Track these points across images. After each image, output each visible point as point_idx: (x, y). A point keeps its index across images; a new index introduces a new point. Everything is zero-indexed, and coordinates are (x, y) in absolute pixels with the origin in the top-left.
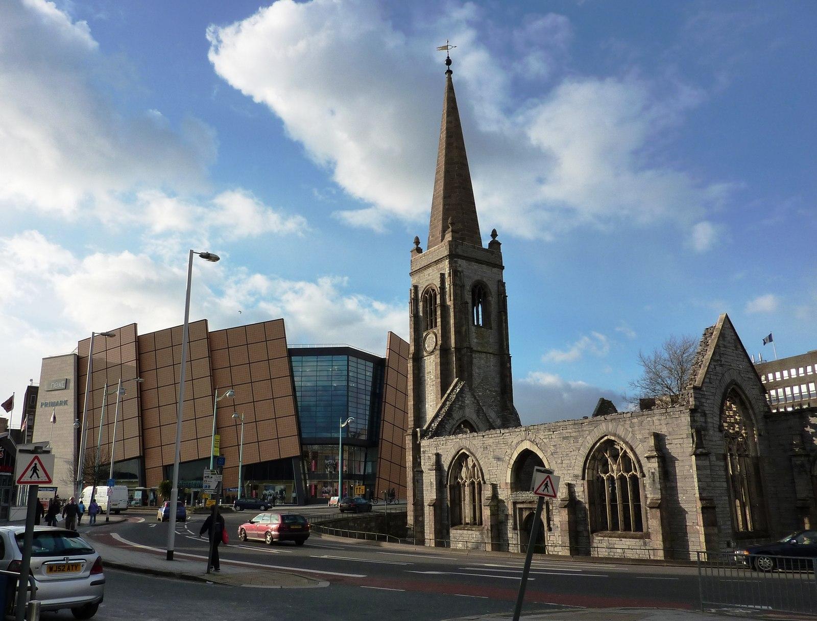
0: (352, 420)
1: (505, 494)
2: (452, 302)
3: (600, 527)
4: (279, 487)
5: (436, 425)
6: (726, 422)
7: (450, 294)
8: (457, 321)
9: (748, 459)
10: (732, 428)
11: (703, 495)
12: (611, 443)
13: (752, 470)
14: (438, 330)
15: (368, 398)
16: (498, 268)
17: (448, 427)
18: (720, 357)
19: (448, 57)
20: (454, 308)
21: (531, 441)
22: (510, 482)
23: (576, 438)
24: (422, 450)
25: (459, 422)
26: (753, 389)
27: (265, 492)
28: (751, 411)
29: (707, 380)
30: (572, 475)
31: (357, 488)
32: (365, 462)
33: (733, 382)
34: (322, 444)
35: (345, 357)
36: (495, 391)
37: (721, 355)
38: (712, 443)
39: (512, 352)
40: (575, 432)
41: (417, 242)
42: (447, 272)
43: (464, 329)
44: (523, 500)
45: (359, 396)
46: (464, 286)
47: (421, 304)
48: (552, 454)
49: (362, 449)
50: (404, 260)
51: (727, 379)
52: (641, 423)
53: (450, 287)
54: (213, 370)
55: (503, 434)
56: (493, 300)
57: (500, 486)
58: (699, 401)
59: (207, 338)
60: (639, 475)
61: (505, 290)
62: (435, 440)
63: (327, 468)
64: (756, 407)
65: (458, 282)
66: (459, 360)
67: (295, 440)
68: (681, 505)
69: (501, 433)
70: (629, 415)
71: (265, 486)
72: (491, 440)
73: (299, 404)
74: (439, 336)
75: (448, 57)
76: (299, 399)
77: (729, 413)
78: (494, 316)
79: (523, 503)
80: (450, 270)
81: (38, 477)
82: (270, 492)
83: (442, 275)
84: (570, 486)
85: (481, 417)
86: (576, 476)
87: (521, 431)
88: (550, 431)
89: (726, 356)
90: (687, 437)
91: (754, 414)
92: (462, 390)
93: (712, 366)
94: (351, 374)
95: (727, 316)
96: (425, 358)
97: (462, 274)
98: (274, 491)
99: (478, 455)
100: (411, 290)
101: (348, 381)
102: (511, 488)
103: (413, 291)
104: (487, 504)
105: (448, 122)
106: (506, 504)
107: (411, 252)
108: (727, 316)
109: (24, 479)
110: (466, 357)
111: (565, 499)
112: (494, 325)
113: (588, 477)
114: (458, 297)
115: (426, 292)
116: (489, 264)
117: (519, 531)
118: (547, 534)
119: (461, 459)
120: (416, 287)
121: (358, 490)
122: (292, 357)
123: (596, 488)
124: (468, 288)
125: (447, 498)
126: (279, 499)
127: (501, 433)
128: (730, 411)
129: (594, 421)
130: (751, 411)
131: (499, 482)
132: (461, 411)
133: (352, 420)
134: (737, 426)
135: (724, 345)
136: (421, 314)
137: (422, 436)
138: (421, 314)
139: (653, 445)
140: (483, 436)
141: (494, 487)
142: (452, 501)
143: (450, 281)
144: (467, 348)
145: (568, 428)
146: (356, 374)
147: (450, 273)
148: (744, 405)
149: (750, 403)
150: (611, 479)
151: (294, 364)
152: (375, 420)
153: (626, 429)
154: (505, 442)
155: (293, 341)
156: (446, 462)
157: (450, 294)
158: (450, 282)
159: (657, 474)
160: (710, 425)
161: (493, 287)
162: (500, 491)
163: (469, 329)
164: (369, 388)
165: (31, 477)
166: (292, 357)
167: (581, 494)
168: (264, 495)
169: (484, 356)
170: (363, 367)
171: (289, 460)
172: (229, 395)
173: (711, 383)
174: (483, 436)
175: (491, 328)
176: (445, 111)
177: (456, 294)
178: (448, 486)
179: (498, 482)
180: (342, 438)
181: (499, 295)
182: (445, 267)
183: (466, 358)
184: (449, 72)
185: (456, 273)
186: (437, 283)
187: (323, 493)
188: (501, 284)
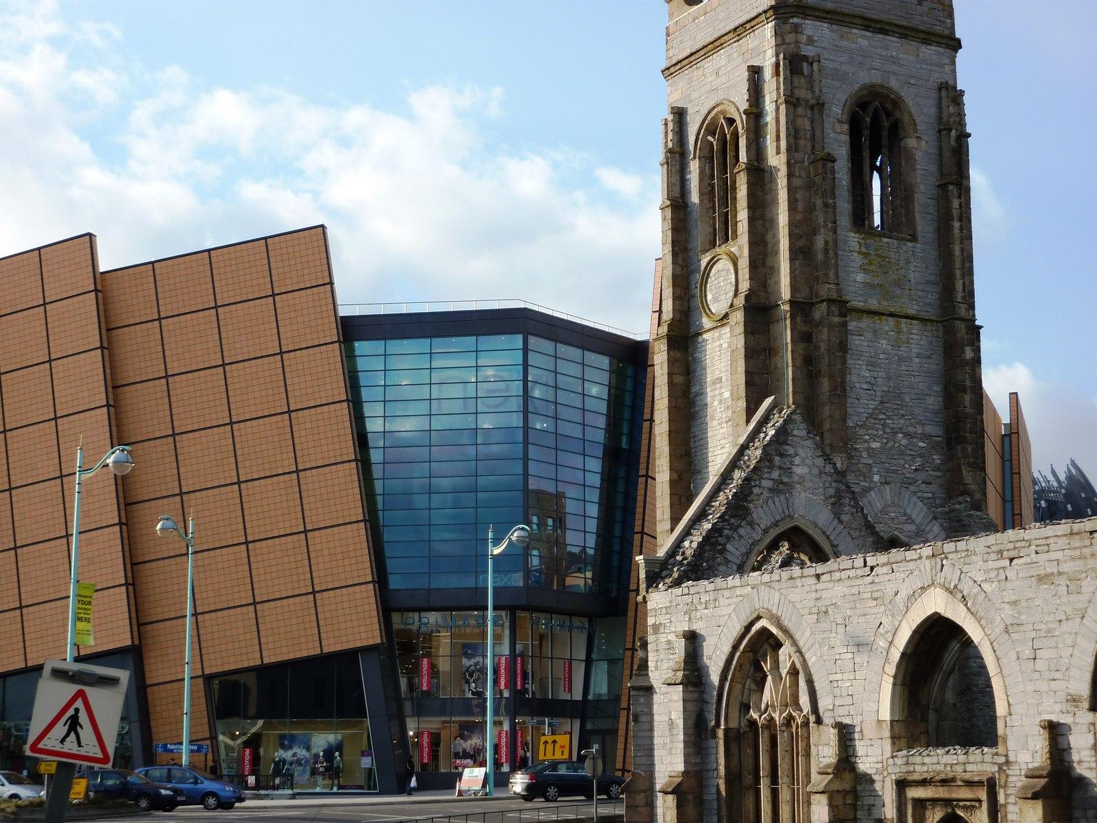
0: (522, 533)
2: (783, 157)
4: (322, 740)
5: (695, 545)
7: (778, 131)
8: (799, 217)
14: (741, 245)
15: (595, 465)
16: (939, 44)
17: (734, 550)
20: (790, 176)
21: (947, 590)
24: (651, 621)
25: (774, 533)
27: (281, 754)
30: (1062, 696)
31: (546, 742)
32: (589, 662)
34: (451, 609)
35: (518, 340)
36: (926, 437)
39: (982, 316)
40: (1073, 559)
42: (768, 61)
43: (819, 241)
44: (926, 776)
45: (564, 458)
46: (823, 105)
47: (694, 167)
49: (577, 622)
54: (115, 387)
55: (872, 568)
57: (861, 731)
59: (96, 290)
61: (961, 115)
62: (686, 591)
63: (468, 682)
65: (802, 93)
66: (804, 338)
67: (367, 597)
69: (865, 565)
71: (282, 737)
72: (840, 589)
73: (378, 486)
74: (744, 263)
76: (377, 472)
79: (924, 783)
80: (777, 55)
81: (79, 744)
82: (294, 755)
83: (755, 73)
84: (1055, 731)
85: (845, 518)
86: (1074, 700)
87: (920, 558)
92: (782, 432)
94: (537, 393)
96: (705, 336)
97: (815, 66)
98: (308, 749)
99: (803, 639)
100: (666, 124)
101: (526, 412)
102: (894, 738)
103: (671, 126)
104: (821, 788)
106: (878, 786)
109: (46, 744)
110: (825, 330)
111: (1036, 773)
112: (924, 225)
115: (711, 127)
120: (680, 115)
121: (550, 747)
122: (356, 344)
124: (837, 109)
125: (717, 769)
126: (323, 774)
127: (865, 565)
131: (860, 717)
132: (779, 501)
133: (522, 533)
136: (695, 198)
137: (654, 579)
138: (695, 198)
140: (818, 576)
141: (845, 734)
142: (733, 778)
143: (778, 89)
144: (830, 301)
145: (1052, 547)
146: (552, 391)
147: (777, 65)
151: (361, 364)
152: (617, 532)
154: (875, 595)
156: (715, 659)
157: (778, 131)
158: (778, 94)
162: (861, 748)
163: (836, 242)
164: (600, 436)
165: (63, 741)
166: (356, 344)
168: (277, 764)
169: (888, 324)
170: (575, 370)
171: (349, 657)
172: (114, 462)
174: (818, 576)
175: (914, 238)
177: (797, 131)
178: (721, 733)
179: (856, 721)
180: (495, 588)
181: (940, 131)
183: (824, 334)
186: (741, 99)
187: (457, 756)
188: (951, 97)
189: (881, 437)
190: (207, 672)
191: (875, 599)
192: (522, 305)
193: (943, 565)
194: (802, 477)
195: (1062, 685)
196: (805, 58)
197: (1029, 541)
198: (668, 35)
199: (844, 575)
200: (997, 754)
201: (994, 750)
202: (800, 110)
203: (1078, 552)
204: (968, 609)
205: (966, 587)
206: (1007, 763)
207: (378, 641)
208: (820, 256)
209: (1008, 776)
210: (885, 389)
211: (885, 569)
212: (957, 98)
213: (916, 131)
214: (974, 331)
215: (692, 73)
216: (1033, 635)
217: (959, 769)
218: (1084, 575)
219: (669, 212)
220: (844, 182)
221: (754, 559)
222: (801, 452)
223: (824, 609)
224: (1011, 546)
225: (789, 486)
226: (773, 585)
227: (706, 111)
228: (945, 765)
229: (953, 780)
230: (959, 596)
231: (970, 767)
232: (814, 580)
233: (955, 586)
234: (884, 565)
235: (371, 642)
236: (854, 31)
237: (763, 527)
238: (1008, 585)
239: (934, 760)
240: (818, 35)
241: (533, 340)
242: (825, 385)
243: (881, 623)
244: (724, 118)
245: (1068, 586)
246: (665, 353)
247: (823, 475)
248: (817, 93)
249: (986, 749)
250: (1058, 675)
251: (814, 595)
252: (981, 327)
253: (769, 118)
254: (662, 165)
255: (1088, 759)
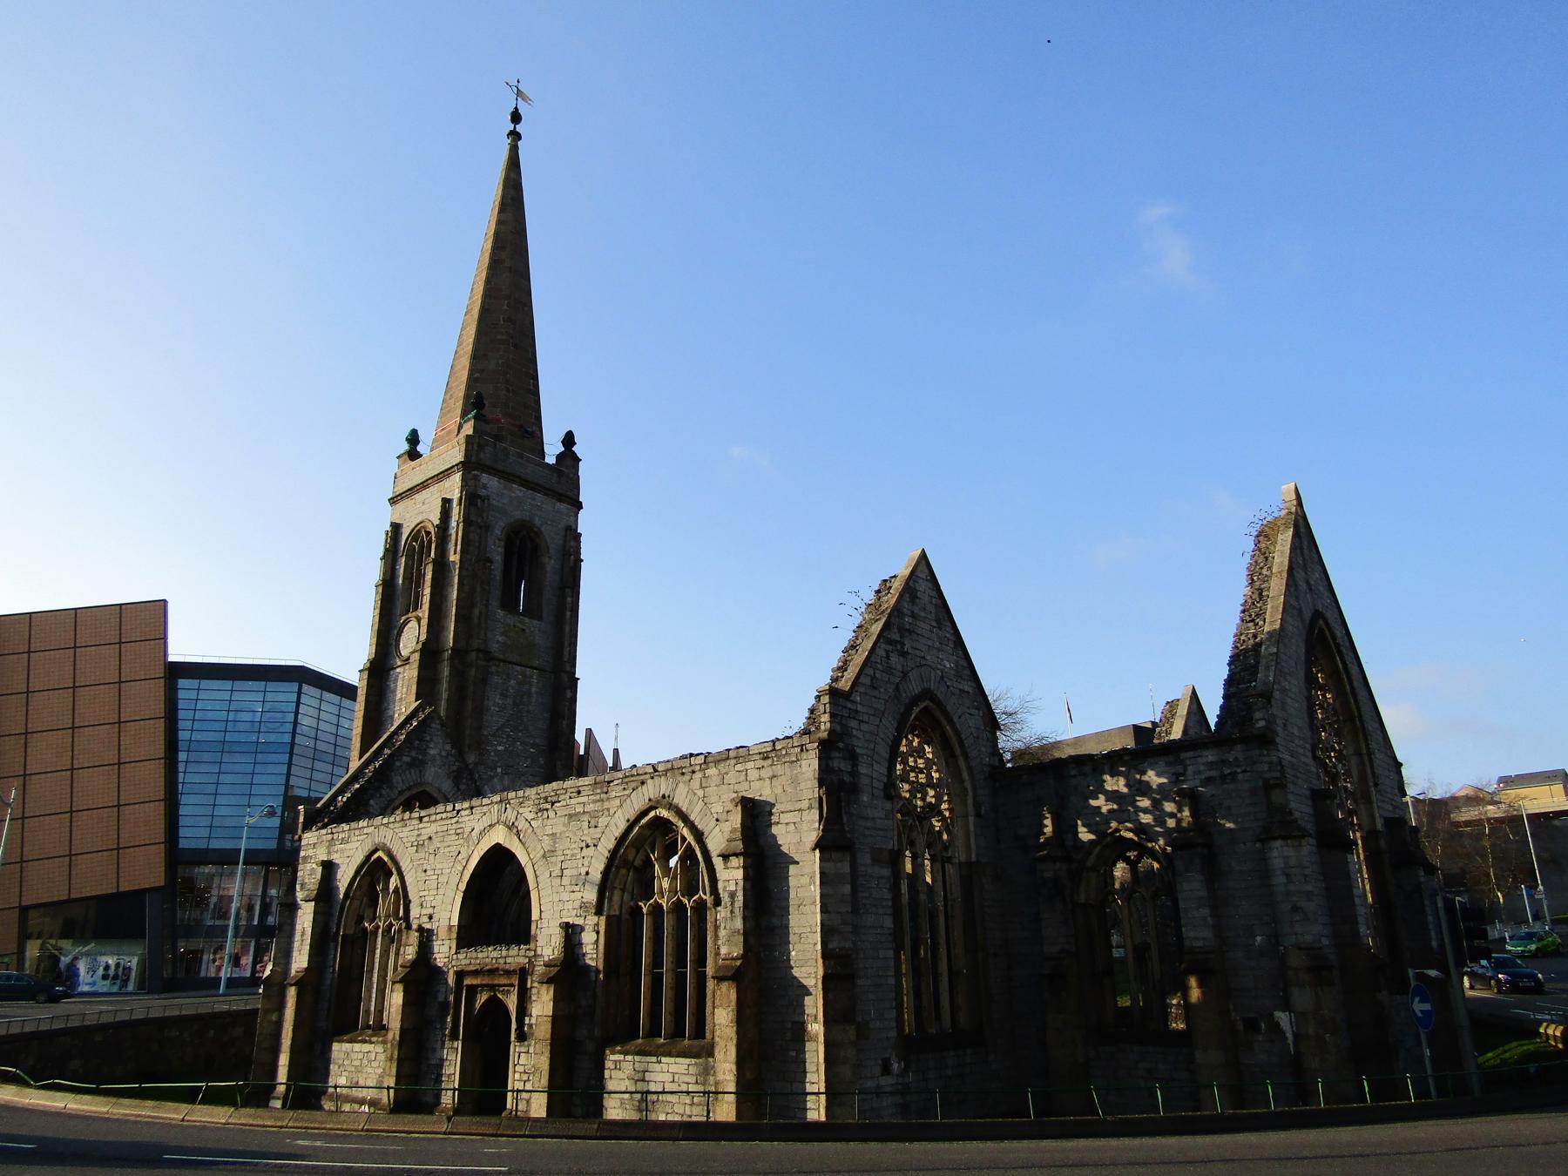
1: (443, 951)
3: (623, 1034)
6: (908, 782)
7: (457, 540)
9: (950, 866)
10: (919, 795)
11: (831, 946)
12: (662, 825)
13: (956, 891)
14: (424, 611)
18: (902, 636)
19: (516, 108)
22: (456, 924)
23: (594, 815)
26: (970, 714)
28: (961, 762)
29: (865, 680)
33: (927, 694)
35: (295, 686)
37: (903, 631)
38: (869, 824)
39: (580, 671)
40: (595, 802)
41: (413, 439)
42: (455, 495)
45: (318, 765)
48: (544, 856)
50: (385, 471)
51: (915, 687)
52: (722, 776)
53: (458, 525)
55: (458, 812)
56: (551, 564)
58: (841, 723)
60: (708, 898)
64: (973, 754)
65: (474, 518)
67: (157, 855)
68: (796, 972)
70: (701, 759)
74: (424, 622)
75: (516, 108)
77: (916, 762)
78: (548, 595)
80: (461, 493)
83: (446, 503)
86: (583, 906)
87: (492, 803)
88: (547, 802)
89: (915, 637)
90: (810, 808)
91: (970, 769)
93: (881, 652)
95: (923, 556)
97: (486, 501)
100: (387, 534)
105: (499, 223)
107: (398, 457)
108: (923, 556)
110: (474, 670)
111: (553, 963)
113: (609, 909)
114: (471, 549)
115: (416, 535)
116: (548, 492)
117: (460, 1042)
118: (515, 1048)
119: (376, 870)
120: (396, 528)
123: (622, 934)
124: (498, 531)
127: (454, 810)
128: (920, 758)
129: (632, 776)
130: (961, 762)
131: (437, 923)
134: (931, 793)
135: (912, 612)
139: (739, 826)
140: (421, 819)
141: (426, 937)
143: (460, 513)
144: (479, 650)
147: (461, 498)
148: (949, 752)
149: (961, 742)
150: (657, 909)
151: (181, 694)
153: (692, 790)
154: (458, 831)
155: (179, 650)
157: (457, 540)
159: (740, 897)
160: (864, 781)
161: (552, 538)
167: (592, 946)
171: (139, 894)
173: (876, 689)
174: (421, 819)
176: (497, 203)
181: (564, 555)
182: (453, 487)
183: (473, 672)
184: (515, 136)
185: (472, 498)
188: (572, 538)
189: (505, 743)
190: (23, 904)
191: (458, 834)
192: (301, 664)
193: (506, 808)
194: (434, 756)
195: (578, 895)
196: (480, 497)
197: (566, 789)
198: (395, 478)
199: (438, 817)
200: (529, 949)
201: (528, 947)
202: (472, 528)
203: (598, 797)
204: (520, 840)
205: (522, 825)
206: (535, 956)
207: (162, 884)
208: (476, 621)
209: (534, 966)
210: (511, 712)
211: (467, 812)
212: (577, 537)
213: (548, 552)
214: (574, 682)
215: (407, 503)
216: (563, 858)
217: (502, 961)
218: (601, 813)
219: (380, 589)
220: (498, 578)
221: (389, 811)
222: (435, 739)
223: (421, 842)
224: (553, 794)
225: (423, 763)
226: (391, 826)
227: (415, 523)
228: (492, 959)
229: (497, 969)
230: (515, 830)
231: (509, 960)
232: (416, 822)
233: (513, 824)
234: (466, 809)
235: (157, 885)
236: (514, 486)
237: (400, 789)
238: (549, 822)
239: (485, 954)
240: (491, 483)
241: (305, 688)
242: (469, 705)
243: (459, 852)
244: (425, 531)
245: (589, 822)
246: (366, 681)
247: (450, 757)
248: (485, 518)
249: (522, 946)
250: (577, 888)
251: (416, 832)
252: (578, 679)
253: (453, 532)
254: (381, 559)
255: (592, 952)
